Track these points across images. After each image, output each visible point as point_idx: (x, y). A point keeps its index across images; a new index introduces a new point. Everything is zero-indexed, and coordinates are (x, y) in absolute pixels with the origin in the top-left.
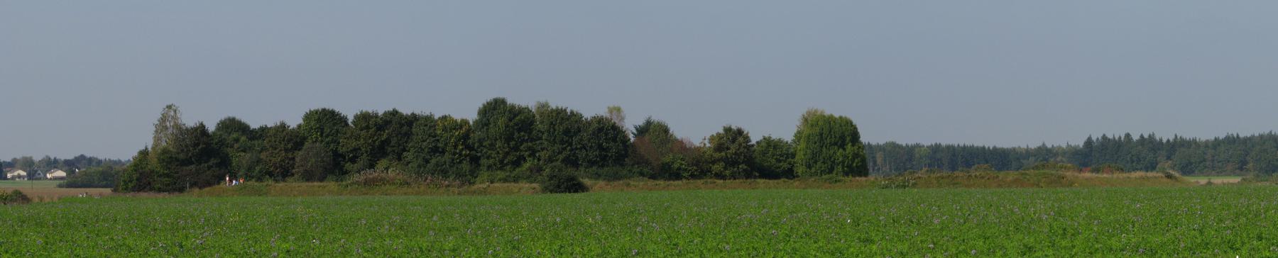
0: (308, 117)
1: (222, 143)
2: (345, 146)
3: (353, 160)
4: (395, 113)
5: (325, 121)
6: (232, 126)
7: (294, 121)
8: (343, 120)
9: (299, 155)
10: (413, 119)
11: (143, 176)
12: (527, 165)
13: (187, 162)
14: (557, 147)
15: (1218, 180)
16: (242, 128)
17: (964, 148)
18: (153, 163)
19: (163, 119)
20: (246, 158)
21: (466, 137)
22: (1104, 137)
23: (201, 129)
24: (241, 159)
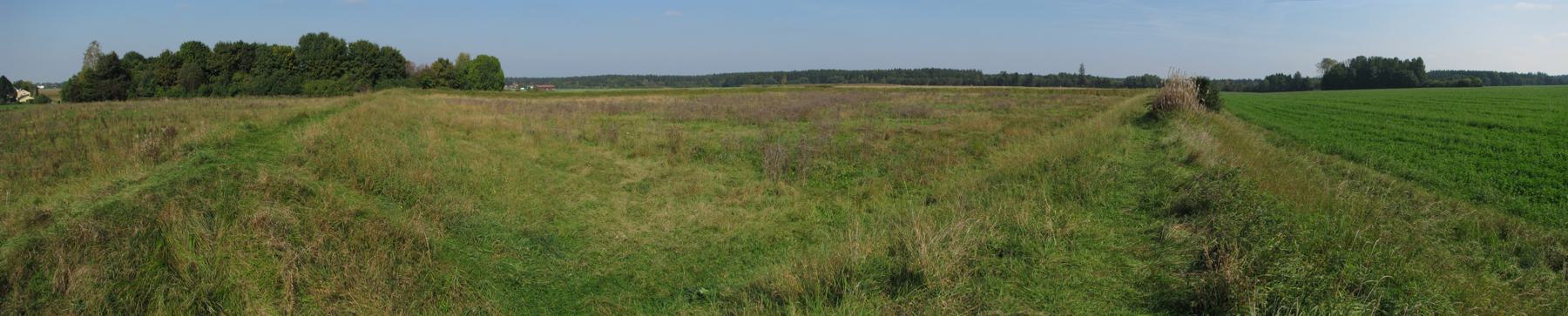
0: (184, 46)
1: (127, 65)
2: (211, 64)
3: (217, 74)
4: (241, 43)
5: (195, 49)
6: (134, 56)
7: (175, 49)
8: (206, 49)
9: (181, 71)
10: (254, 47)
11: (75, 91)
12: (345, 76)
13: (105, 77)
14: (366, 64)
15: (534, 101)
16: (140, 57)
17: (1378, 60)
18: (81, 80)
19: (89, 50)
20: (143, 74)
21: (293, 58)
22: (1298, 75)
23: (114, 56)
24: (139, 75)
